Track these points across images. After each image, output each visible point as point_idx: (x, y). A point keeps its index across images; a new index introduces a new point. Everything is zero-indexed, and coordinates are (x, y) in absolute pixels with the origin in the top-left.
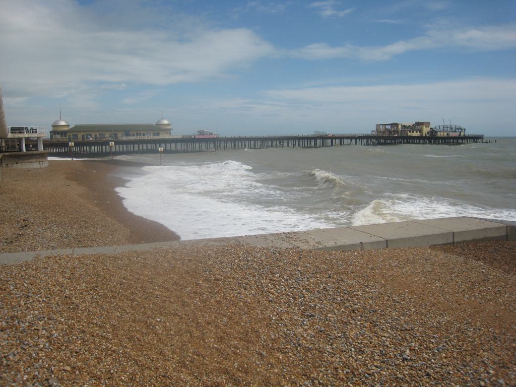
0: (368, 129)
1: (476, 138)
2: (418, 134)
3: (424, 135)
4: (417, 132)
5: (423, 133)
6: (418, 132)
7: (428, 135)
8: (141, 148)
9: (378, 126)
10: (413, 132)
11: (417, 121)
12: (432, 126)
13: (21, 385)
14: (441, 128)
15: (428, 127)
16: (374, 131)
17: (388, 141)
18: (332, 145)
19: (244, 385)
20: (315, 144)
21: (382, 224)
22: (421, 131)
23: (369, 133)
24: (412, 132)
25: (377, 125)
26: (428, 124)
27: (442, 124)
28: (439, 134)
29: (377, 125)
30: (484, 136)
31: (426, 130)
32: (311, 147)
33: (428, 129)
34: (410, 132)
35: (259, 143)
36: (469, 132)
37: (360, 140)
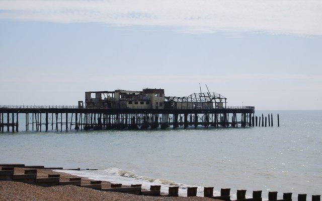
2: (145, 106)
4: (142, 103)
9: (88, 94)
10: (136, 103)
11: (145, 87)
12: (166, 95)
14: (198, 97)
16: (82, 102)
23: (75, 105)
26: (161, 92)
27: (198, 92)
36: (178, 88)
37: (79, 114)
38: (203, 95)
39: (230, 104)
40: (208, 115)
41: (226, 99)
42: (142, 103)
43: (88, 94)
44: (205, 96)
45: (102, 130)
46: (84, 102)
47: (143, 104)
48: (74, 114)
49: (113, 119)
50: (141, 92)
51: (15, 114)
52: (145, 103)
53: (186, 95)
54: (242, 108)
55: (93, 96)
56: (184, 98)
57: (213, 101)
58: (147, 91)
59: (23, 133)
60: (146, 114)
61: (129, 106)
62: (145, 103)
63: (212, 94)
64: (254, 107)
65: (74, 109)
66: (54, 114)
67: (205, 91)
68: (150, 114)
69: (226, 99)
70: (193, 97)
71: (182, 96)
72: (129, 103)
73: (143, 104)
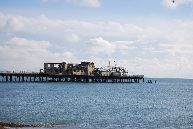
0: (37, 67)
2: (83, 73)
3: (89, 74)
4: (82, 72)
5: (87, 72)
7: (92, 75)
9: (46, 65)
10: (78, 71)
12: (96, 66)
14: (108, 68)
15: (92, 67)
16: (43, 69)
20: (60, 80)
22: (86, 70)
23: (38, 71)
24: (77, 71)
25: (45, 64)
29: (45, 64)
31: (90, 70)
33: (93, 69)
34: (75, 71)
36: (132, 72)
38: (111, 67)
39: (130, 74)
40: (118, 78)
41: (127, 70)
43: (46, 65)
44: (113, 68)
45: (101, 82)
47: (82, 72)
50: (80, 64)
51: (40, 77)
52: (83, 71)
54: (10, 72)
55: (49, 66)
56: (98, 69)
57: (121, 71)
58: (83, 64)
62: (83, 71)
63: (118, 67)
66: (17, 77)
68: (69, 79)
69: (127, 70)
72: (78, 72)
73: (82, 72)
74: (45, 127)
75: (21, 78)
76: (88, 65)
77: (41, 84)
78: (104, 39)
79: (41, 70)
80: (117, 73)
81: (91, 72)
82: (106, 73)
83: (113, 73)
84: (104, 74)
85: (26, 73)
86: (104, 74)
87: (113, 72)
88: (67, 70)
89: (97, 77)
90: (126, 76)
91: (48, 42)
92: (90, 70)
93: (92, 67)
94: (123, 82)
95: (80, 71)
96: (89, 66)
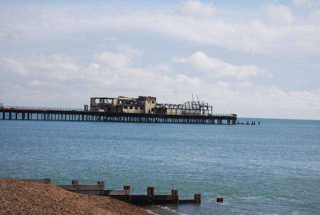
0: (80, 102)
1: (232, 119)
2: (139, 111)
3: (147, 111)
4: (136, 108)
5: (145, 110)
6: (139, 108)
7: (152, 113)
8: (159, 120)
9: (93, 100)
12: (158, 101)
13: (167, 107)
14: (190, 104)
15: (153, 103)
17: (115, 118)
18: (10, 119)
19: (4, 213)
20: (188, 121)
21: (202, 52)
22: (143, 107)
23: (82, 108)
24: (129, 108)
25: (91, 99)
26: (153, 99)
28: (168, 112)
29: (91, 99)
30: (237, 117)
31: (149, 106)
32: (45, 120)
33: (153, 106)
34: (126, 108)
35: (20, 116)
36: (217, 110)
37: (74, 115)
39: (216, 112)
40: (196, 116)
41: (212, 107)
42: (131, 108)
43: (93, 100)
46: (89, 105)
48: (60, 115)
49: (109, 118)
50: (137, 99)
51: (30, 114)
53: (181, 103)
54: (25, 108)
56: (179, 105)
59: (7, 119)
60: (140, 118)
61: (125, 111)
64: (236, 115)
65: (82, 112)
66: (71, 115)
67: (196, 100)
70: (187, 104)
71: (178, 104)
72: (130, 108)
74: (210, 191)
75: (81, 116)
76: (146, 100)
77: (199, 127)
78: (209, 55)
79: (85, 106)
80: (194, 111)
81: (151, 109)
82: (174, 111)
83: (187, 111)
84: (171, 112)
85: (56, 110)
86: (171, 112)
87: (186, 110)
88: (117, 107)
89: (161, 114)
90: (209, 115)
91: (203, 53)
92: (149, 106)
93: (153, 103)
94: (46, 119)
95: (134, 108)
96: (147, 102)
